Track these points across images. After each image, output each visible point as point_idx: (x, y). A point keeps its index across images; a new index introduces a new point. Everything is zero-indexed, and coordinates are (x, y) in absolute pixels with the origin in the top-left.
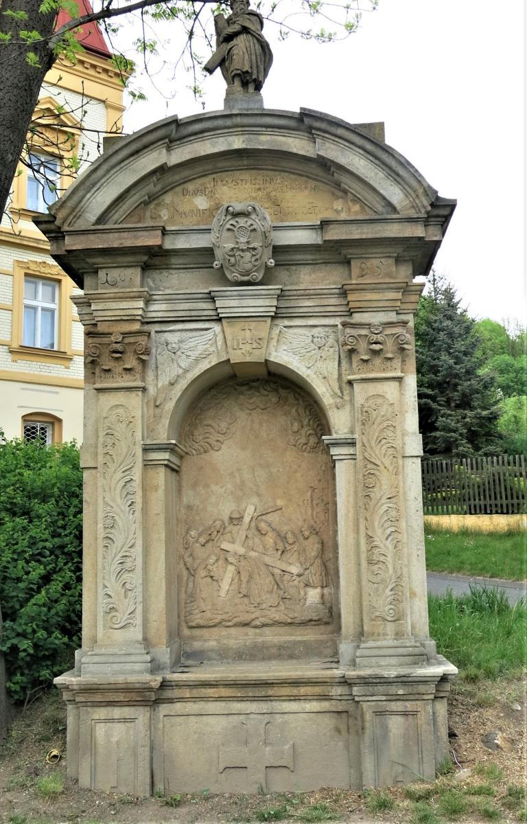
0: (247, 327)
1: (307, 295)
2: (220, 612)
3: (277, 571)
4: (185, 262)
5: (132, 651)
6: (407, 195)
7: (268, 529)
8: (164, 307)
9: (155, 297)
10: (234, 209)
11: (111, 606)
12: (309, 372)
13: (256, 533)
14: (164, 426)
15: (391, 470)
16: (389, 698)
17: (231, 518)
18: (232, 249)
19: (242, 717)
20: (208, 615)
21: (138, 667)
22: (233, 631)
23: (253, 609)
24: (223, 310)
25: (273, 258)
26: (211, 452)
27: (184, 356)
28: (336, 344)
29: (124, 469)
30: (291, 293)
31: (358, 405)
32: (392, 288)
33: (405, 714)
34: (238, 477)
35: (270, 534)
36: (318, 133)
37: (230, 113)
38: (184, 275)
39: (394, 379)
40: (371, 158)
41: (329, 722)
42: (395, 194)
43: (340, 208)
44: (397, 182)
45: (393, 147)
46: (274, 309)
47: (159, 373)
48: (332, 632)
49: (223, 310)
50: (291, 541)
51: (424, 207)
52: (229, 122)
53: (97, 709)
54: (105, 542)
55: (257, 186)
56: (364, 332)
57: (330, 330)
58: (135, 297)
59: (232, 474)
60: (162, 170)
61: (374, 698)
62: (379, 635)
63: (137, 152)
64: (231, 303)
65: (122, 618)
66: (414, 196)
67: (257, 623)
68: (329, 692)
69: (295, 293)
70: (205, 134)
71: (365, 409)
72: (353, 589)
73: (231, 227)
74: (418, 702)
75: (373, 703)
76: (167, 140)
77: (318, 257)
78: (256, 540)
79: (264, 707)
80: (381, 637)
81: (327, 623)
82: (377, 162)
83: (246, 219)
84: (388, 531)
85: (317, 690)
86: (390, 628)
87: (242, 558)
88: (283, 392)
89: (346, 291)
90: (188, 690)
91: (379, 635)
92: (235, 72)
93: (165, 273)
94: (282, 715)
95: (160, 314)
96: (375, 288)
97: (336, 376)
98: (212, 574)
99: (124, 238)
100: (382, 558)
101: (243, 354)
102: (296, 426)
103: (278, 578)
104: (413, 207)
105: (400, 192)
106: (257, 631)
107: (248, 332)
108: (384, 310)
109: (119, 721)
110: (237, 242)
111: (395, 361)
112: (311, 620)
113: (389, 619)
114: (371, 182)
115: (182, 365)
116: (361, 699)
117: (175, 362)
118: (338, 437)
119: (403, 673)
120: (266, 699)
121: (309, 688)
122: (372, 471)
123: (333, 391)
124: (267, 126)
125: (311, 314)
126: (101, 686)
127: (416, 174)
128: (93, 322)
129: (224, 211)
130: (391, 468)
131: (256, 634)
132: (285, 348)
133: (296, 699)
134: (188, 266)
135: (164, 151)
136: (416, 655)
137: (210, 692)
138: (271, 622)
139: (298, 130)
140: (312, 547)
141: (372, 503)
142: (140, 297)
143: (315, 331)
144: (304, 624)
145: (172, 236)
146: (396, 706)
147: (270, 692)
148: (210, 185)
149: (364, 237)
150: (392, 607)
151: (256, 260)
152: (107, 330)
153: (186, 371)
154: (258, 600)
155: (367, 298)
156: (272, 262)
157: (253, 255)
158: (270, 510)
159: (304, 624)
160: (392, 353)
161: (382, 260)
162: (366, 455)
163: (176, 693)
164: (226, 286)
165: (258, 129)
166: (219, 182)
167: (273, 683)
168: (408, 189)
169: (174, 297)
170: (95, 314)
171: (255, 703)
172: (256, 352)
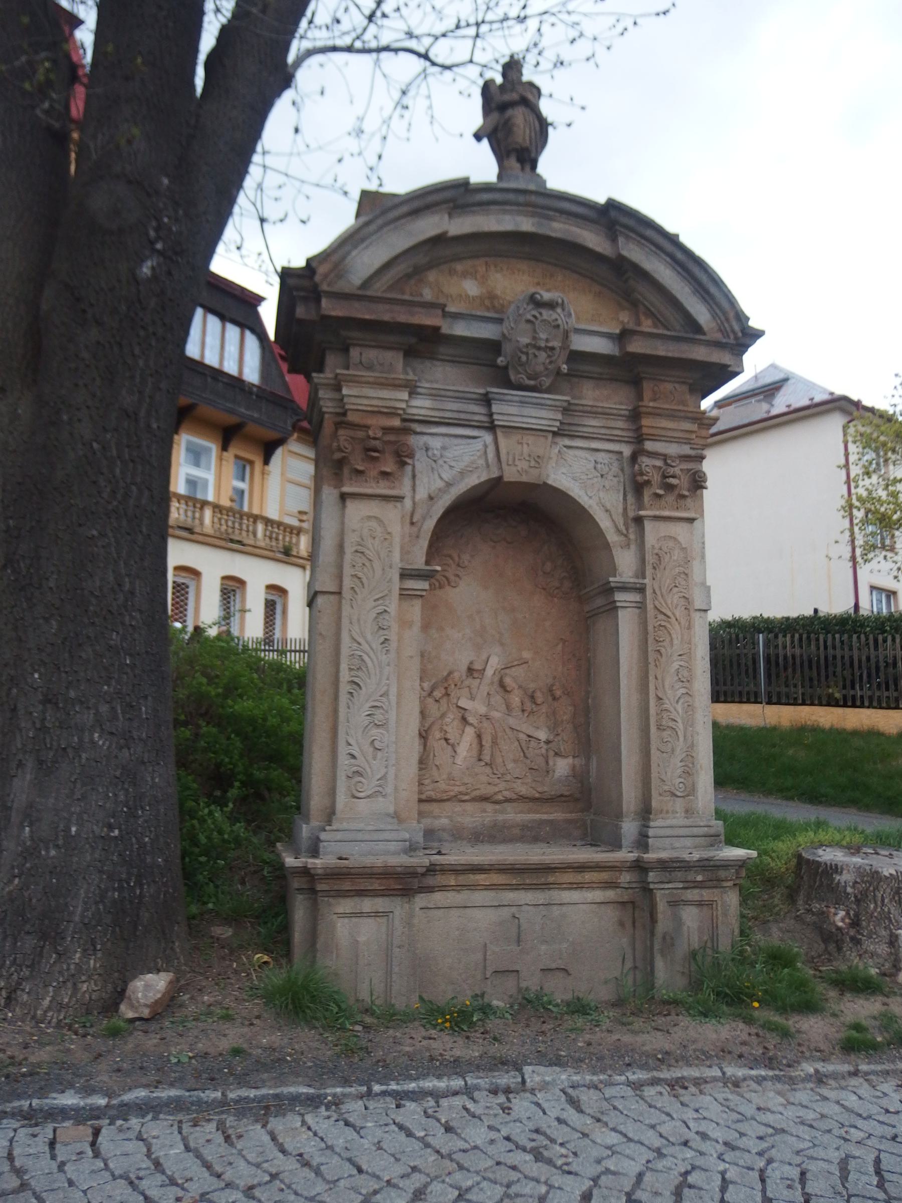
0: (525, 441)
1: (594, 413)
2: (458, 783)
3: (522, 736)
5: (382, 827)
6: (714, 316)
7: (514, 685)
8: (427, 403)
9: (419, 390)
10: (541, 296)
11: (355, 769)
13: (499, 689)
16: (686, 885)
18: (527, 345)
19: (514, 909)
20: (442, 786)
21: (393, 846)
22: (469, 807)
23: (498, 781)
25: (566, 363)
26: (448, 588)
27: (446, 467)
29: (377, 597)
30: (577, 408)
31: (648, 546)
33: (700, 904)
35: (516, 691)
36: (622, 230)
40: (679, 269)
41: (611, 915)
42: (701, 313)
46: (558, 424)
48: (582, 811)
50: (539, 701)
52: (521, 199)
53: (342, 900)
54: (349, 688)
56: (659, 463)
57: (614, 457)
60: (440, 240)
61: (670, 886)
62: (667, 812)
65: (368, 787)
67: (500, 797)
68: (617, 879)
69: (581, 408)
71: (656, 551)
74: (714, 890)
75: (667, 892)
76: (451, 205)
79: (540, 897)
81: (577, 800)
83: (551, 312)
85: (604, 876)
86: (679, 805)
90: (453, 877)
91: (667, 812)
93: (428, 363)
94: (559, 907)
95: (422, 412)
97: (621, 510)
100: (671, 724)
102: (548, 566)
103: (523, 745)
106: (497, 807)
107: (525, 446)
108: (679, 441)
109: (369, 915)
111: (689, 500)
112: (562, 796)
113: (679, 794)
115: (444, 476)
116: (656, 886)
117: (436, 472)
118: (623, 580)
119: (706, 856)
120: (546, 886)
121: (595, 874)
122: (663, 623)
125: (595, 436)
126: (352, 871)
130: (683, 621)
131: (496, 811)
132: (564, 470)
133: (579, 886)
134: (457, 359)
135: (446, 217)
136: (712, 836)
137: (481, 878)
138: (515, 797)
140: (565, 711)
141: (664, 659)
142: (406, 386)
143: (601, 456)
146: (693, 895)
147: (551, 879)
148: (482, 269)
149: (670, 354)
150: (682, 780)
151: (551, 362)
153: (449, 485)
154: (502, 770)
155: (662, 425)
156: (565, 368)
158: (516, 663)
162: (656, 603)
163: (440, 879)
164: (498, 387)
166: (492, 268)
167: (556, 868)
168: (718, 311)
169: (443, 393)
170: (346, 400)
171: (531, 891)
172: (532, 470)
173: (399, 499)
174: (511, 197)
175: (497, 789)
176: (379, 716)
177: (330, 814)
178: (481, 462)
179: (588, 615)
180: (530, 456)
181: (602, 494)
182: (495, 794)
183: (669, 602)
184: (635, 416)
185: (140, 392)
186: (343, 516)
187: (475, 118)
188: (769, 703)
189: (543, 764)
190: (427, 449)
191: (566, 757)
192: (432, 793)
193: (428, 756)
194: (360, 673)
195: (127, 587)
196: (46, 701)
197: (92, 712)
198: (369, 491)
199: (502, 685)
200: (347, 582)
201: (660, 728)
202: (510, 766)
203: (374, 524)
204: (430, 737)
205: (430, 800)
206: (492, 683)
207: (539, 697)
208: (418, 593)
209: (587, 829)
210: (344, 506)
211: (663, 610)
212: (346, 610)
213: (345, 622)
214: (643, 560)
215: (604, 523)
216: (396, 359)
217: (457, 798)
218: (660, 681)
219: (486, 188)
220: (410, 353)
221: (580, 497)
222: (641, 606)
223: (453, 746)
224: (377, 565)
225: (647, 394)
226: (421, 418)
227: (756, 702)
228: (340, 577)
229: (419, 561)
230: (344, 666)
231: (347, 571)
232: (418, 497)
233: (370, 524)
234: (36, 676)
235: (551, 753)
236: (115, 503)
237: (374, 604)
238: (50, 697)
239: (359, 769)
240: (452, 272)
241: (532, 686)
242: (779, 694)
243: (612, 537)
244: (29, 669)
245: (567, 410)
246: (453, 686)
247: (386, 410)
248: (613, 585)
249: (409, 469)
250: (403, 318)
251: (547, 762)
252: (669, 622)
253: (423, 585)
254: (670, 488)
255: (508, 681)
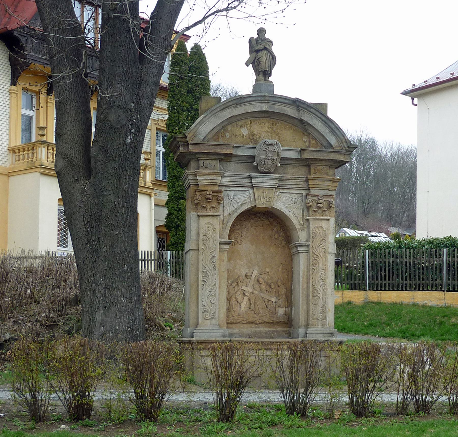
1: (291, 180)
3: (266, 300)
4: (238, 160)
8: (228, 179)
9: (225, 175)
10: (268, 142)
11: (205, 310)
12: (290, 213)
14: (227, 233)
15: (323, 258)
17: (246, 276)
20: (236, 317)
21: (218, 335)
24: (255, 184)
28: (302, 202)
29: (211, 251)
30: (284, 178)
31: (311, 230)
32: (328, 180)
34: (249, 257)
37: (264, 95)
38: (237, 165)
39: (326, 219)
40: (324, 123)
42: (333, 140)
43: (306, 140)
44: (334, 135)
45: (334, 120)
46: (277, 185)
47: (225, 209)
48: (289, 327)
49: (255, 184)
51: (345, 147)
52: (262, 99)
54: (202, 283)
55: (270, 126)
56: (315, 198)
58: (218, 175)
59: (246, 256)
62: (315, 325)
63: (223, 109)
64: (258, 180)
66: (341, 142)
69: (286, 178)
70: (251, 102)
71: (314, 232)
72: (305, 307)
73: (265, 150)
77: (296, 162)
78: (257, 286)
80: (316, 326)
82: (326, 125)
84: (321, 284)
86: (320, 322)
87: (251, 294)
88: (271, 220)
89: (308, 180)
91: (315, 325)
92: (261, 70)
93: (228, 163)
95: (227, 183)
96: (321, 180)
97: (301, 216)
98: (238, 300)
99: (216, 149)
100: (318, 295)
101: (262, 204)
102: (277, 236)
103: (266, 303)
104: (340, 147)
105: (335, 139)
110: (267, 156)
111: (327, 212)
112: (280, 322)
113: (320, 319)
114: (323, 134)
123: (300, 223)
124: (278, 102)
127: (343, 134)
128: (197, 184)
129: (263, 142)
131: (256, 327)
132: (280, 202)
139: (291, 105)
140: (283, 291)
144: (277, 323)
145: (236, 149)
151: (273, 164)
152: (205, 189)
153: (236, 209)
157: (272, 162)
158: (264, 273)
159: (277, 323)
160: (327, 209)
161: (324, 167)
162: (313, 251)
165: (275, 103)
166: (253, 123)
168: (339, 139)
172: (268, 203)
173: (218, 216)
174: (259, 98)
175: (256, 319)
176: (213, 293)
177: (197, 325)
178: (248, 200)
179: (292, 254)
180: (266, 197)
181: (294, 210)
182: (256, 321)
183: (318, 251)
184: (307, 180)
185: (128, 183)
186: (199, 223)
187: (246, 55)
188: (449, 291)
189: (274, 310)
190: (228, 196)
191: (283, 308)
192: (232, 320)
193: (231, 307)
194: (206, 278)
195: (128, 250)
196: (105, 288)
197: (120, 291)
198: (208, 214)
199: (258, 281)
200: (201, 247)
201: (313, 296)
202: (261, 311)
203: (210, 225)
204: (231, 300)
205: (231, 323)
206: (255, 281)
207: (272, 285)
208: (226, 249)
209: (290, 334)
210: (199, 219)
211: (316, 254)
212: (201, 256)
213: (200, 260)
214: (309, 235)
215: (295, 221)
216: (216, 163)
217: (241, 322)
218: (314, 279)
219: (249, 96)
220: (221, 160)
221: (285, 212)
222: (308, 252)
223: (240, 304)
224: (211, 240)
225: (312, 171)
226: (226, 185)
227: (441, 290)
228: (198, 244)
229: (226, 239)
230: (200, 276)
231: (201, 242)
232: (225, 215)
233: (208, 225)
234: (102, 280)
235: (277, 306)
236: (123, 222)
237: (210, 254)
238: (107, 286)
239: (207, 310)
240: (237, 126)
241: (270, 281)
242: (454, 286)
243: (298, 227)
244: (99, 278)
245: (281, 179)
246: (240, 282)
247: (213, 184)
248: (297, 245)
249: (222, 205)
250: (218, 151)
251: (275, 310)
252: (318, 258)
253: (228, 246)
254: (319, 208)
255: (260, 280)
